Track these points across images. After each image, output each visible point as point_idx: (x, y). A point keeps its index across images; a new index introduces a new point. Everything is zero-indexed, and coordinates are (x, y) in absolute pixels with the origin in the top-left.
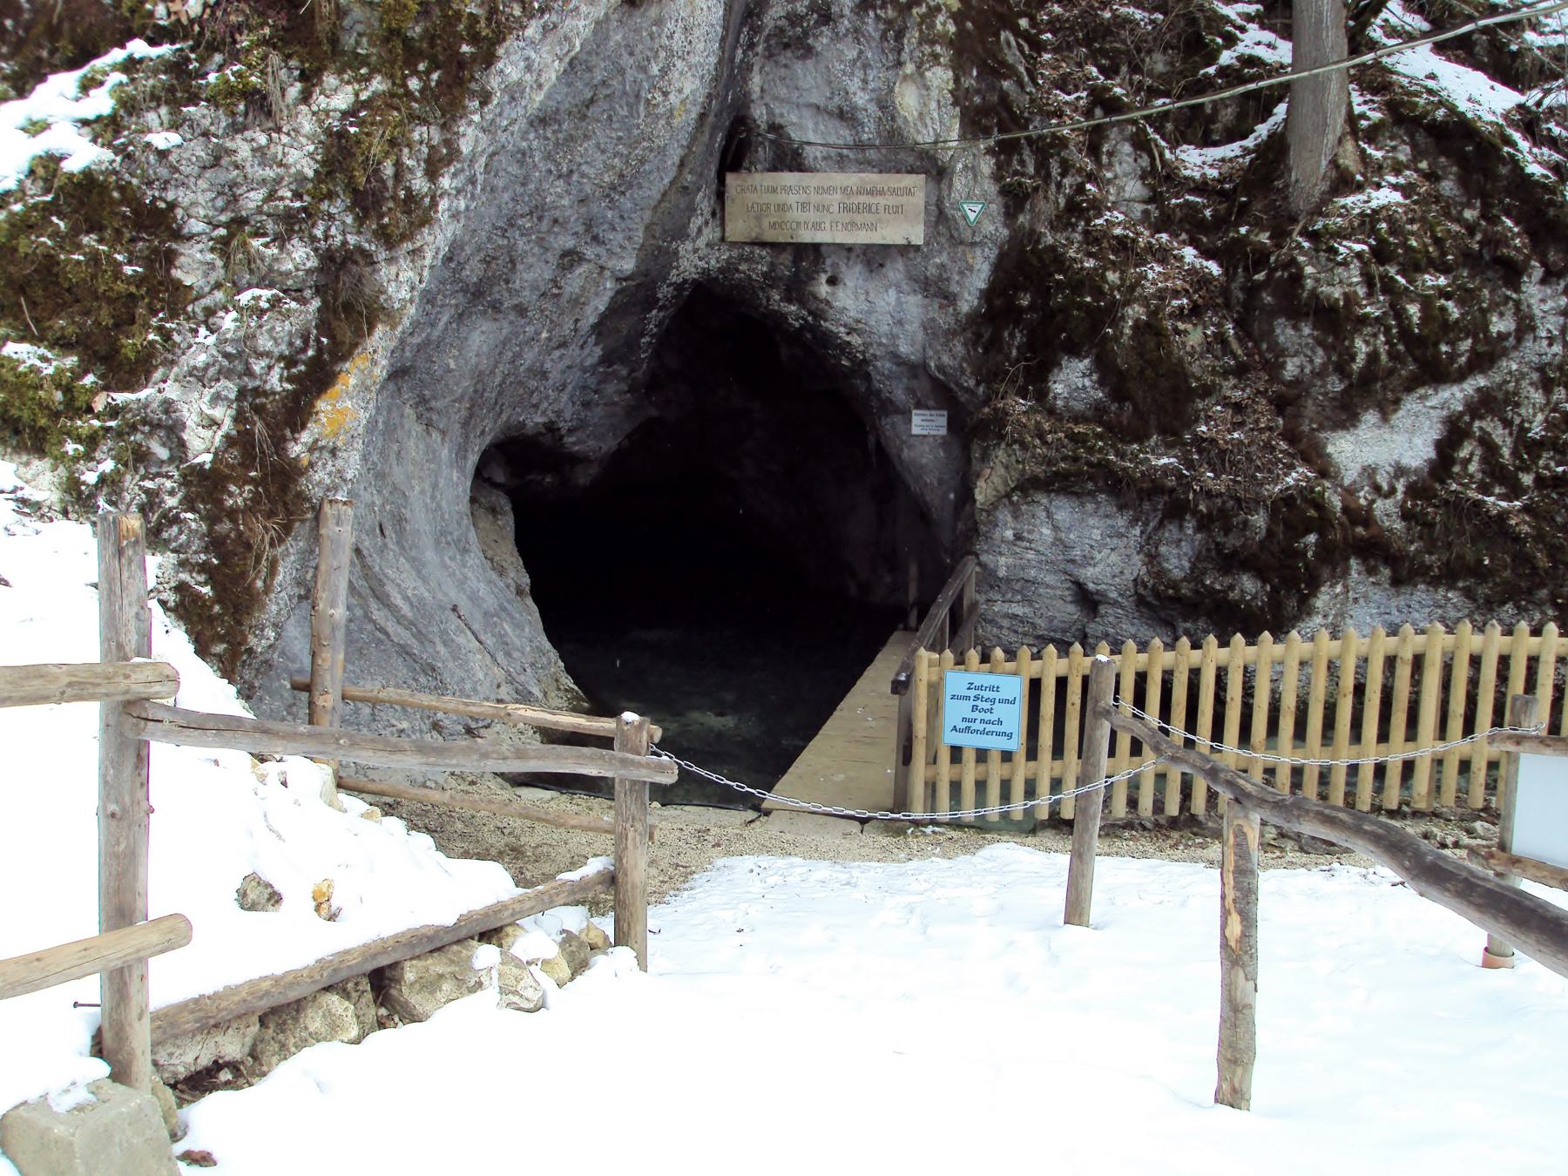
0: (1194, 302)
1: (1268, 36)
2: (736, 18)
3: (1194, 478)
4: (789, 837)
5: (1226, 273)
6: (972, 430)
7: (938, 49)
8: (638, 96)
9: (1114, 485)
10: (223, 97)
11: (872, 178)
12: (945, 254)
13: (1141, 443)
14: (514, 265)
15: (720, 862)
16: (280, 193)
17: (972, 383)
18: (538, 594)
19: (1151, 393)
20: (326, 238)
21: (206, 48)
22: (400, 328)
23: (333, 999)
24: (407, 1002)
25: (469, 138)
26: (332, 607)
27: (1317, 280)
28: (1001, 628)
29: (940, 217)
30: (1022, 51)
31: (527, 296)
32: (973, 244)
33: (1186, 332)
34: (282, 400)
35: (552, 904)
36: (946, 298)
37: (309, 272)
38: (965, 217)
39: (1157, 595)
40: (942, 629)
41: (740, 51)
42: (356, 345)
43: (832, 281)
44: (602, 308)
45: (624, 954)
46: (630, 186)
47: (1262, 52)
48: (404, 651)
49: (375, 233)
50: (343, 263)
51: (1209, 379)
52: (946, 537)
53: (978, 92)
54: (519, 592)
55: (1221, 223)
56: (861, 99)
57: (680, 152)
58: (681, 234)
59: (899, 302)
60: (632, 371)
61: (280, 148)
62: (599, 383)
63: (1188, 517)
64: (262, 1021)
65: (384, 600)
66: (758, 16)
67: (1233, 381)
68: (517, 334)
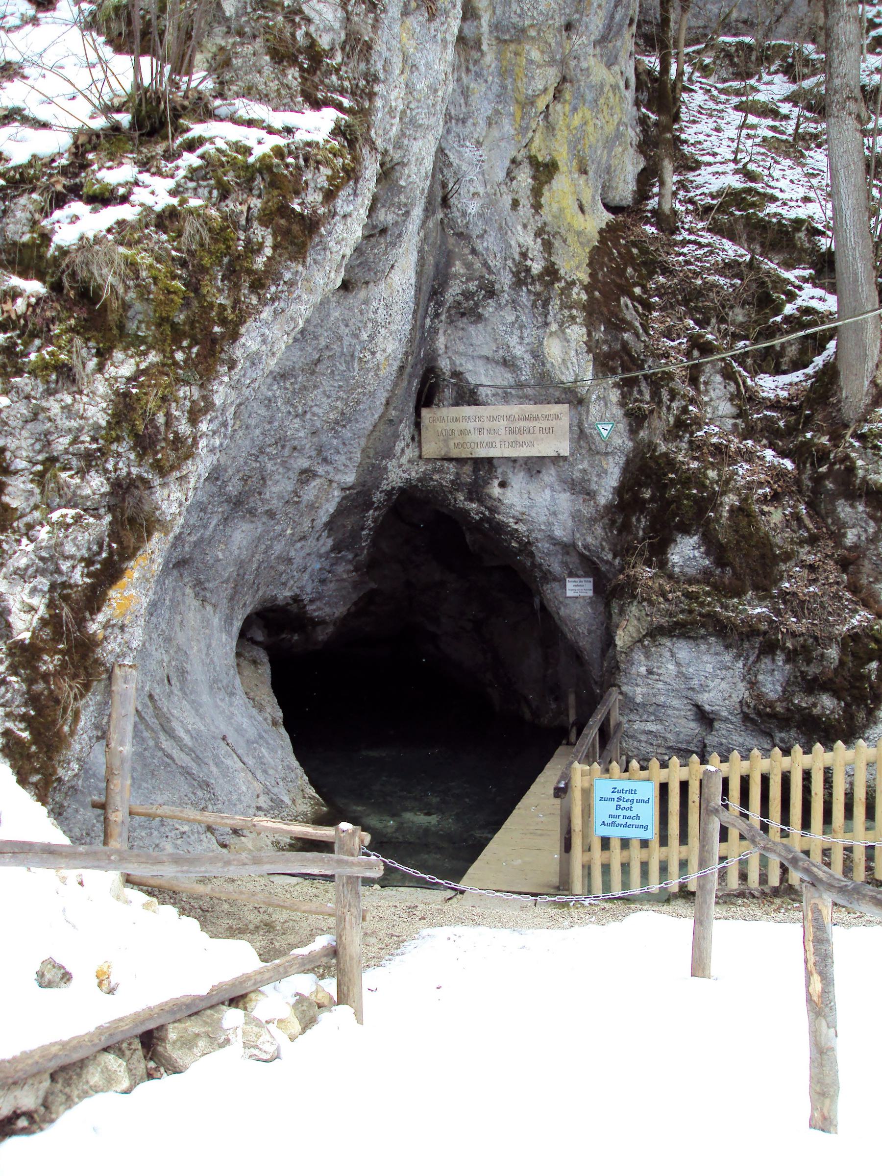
0: (775, 490)
1: (819, 292)
2: (424, 296)
3: (781, 623)
4: (478, 910)
5: (798, 467)
6: (611, 592)
7: (574, 312)
8: (352, 356)
9: (721, 631)
10: (42, 369)
11: (530, 408)
12: (586, 462)
13: (739, 597)
14: (265, 482)
15: (425, 932)
16: (82, 439)
17: (610, 557)
18: (288, 724)
19: (746, 561)
20: (116, 470)
21: (29, 336)
22: (172, 535)
23: (110, 1059)
24: (170, 1057)
25: (221, 393)
26: (121, 745)
27: (867, 470)
28: (640, 741)
29: (581, 435)
30: (637, 311)
31: (275, 504)
32: (607, 454)
33: (769, 513)
34: (83, 590)
35: (286, 974)
36: (588, 494)
37: (103, 495)
38: (599, 434)
39: (759, 713)
40: (593, 745)
41: (428, 320)
42: (138, 549)
43: (503, 485)
44: (332, 511)
45: (345, 1010)
46: (350, 421)
47: (815, 304)
48: (186, 772)
49: (151, 465)
50: (128, 488)
51: (788, 547)
52: (595, 673)
53: (605, 342)
54: (275, 723)
55: (792, 430)
56: (519, 351)
57: (386, 395)
58: (388, 454)
59: (553, 498)
60: (356, 555)
61: (82, 405)
62: (332, 565)
63: (778, 652)
64: (53, 1077)
65: (171, 734)
66: (441, 293)
67: (807, 548)
68: (268, 532)
